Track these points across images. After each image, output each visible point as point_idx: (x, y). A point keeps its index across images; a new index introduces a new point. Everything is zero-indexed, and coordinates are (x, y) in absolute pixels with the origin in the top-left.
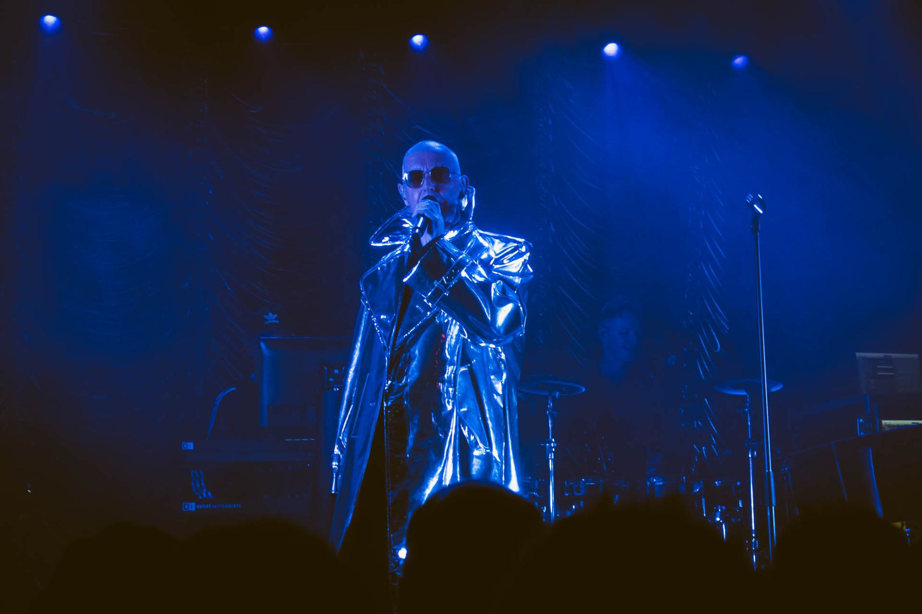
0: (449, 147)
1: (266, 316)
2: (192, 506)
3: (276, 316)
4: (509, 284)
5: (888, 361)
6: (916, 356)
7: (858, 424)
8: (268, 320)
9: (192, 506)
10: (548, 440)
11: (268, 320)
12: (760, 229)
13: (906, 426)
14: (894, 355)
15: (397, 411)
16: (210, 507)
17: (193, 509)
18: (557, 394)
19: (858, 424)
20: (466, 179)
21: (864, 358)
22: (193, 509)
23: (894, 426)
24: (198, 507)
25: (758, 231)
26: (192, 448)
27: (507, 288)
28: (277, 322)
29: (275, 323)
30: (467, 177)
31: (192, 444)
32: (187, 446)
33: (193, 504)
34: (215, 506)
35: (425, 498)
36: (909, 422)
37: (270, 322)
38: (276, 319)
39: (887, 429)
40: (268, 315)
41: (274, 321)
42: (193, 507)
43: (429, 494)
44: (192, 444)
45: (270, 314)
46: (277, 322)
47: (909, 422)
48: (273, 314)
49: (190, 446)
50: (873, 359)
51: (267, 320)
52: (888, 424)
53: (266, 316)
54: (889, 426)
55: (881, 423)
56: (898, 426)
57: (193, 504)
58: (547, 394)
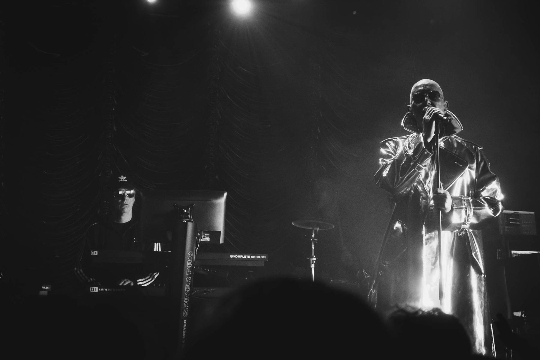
2: (96, 289)
3: (125, 178)
5: (517, 215)
6: (533, 213)
7: (497, 252)
8: (121, 179)
9: (96, 289)
10: (311, 256)
11: (121, 179)
14: (520, 212)
16: (101, 290)
17: (97, 291)
18: (318, 229)
19: (497, 252)
20: (447, 103)
22: (97, 291)
24: (100, 290)
25: (439, 133)
26: (97, 254)
27: (394, 154)
28: (126, 181)
29: (125, 181)
30: (447, 102)
31: (97, 252)
32: (94, 253)
33: (97, 288)
34: (110, 290)
35: (424, 228)
37: (122, 180)
39: (514, 256)
40: (121, 177)
41: (124, 180)
42: (96, 290)
44: (97, 252)
46: (126, 181)
48: (124, 176)
49: (96, 253)
52: (515, 253)
53: (120, 178)
54: (516, 254)
57: (97, 288)
58: (312, 229)
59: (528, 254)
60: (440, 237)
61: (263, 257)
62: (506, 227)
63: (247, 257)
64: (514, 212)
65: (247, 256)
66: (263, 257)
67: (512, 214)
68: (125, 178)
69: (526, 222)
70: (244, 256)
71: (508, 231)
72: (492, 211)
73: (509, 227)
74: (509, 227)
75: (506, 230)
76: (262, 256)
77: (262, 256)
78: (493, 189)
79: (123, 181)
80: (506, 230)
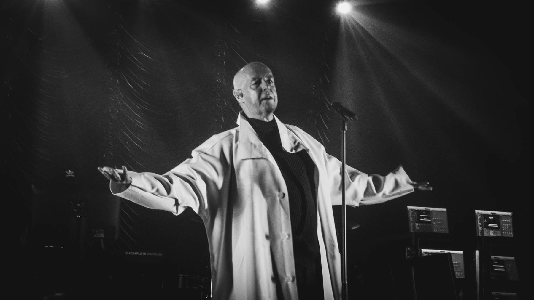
0: (138, 205)
1: (67, 172)
3: (73, 172)
4: (258, 75)
5: (428, 212)
6: (445, 210)
7: (407, 250)
12: (346, 129)
13: (437, 254)
15: (116, 30)
19: (407, 250)
21: (412, 210)
23: (429, 253)
25: (345, 130)
28: (74, 176)
36: (439, 251)
37: (69, 175)
38: (73, 174)
39: (425, 255)
40: (68, 171)
41: (71, 175)
43: (117, 195)
45: (70, 171)
46: (74, 176)
47: (439, 251)
50: (418, 211)
51: (67, 174)
54: (426, 253)
55: (421, 251)
56: (432, 253)
59: (439, 253)
60: (322, 232)
61: (160, 254)
62: (417, 224)
63: (143, 254)
64: (426, 209)
65: (143, 253)
66: (160, 254)
67: (423, 211)
68: (73, 172)
69: (505, 221)
70: (140, 254)
71: (419, 228)
72: (188, 210)
73: (420, 225)
74: (420, 225)
75: (417, 228)
76: (159, 254)
77: (159, 254)
78: (346, 189)
79: (70, 176)
80: (417, 228)
